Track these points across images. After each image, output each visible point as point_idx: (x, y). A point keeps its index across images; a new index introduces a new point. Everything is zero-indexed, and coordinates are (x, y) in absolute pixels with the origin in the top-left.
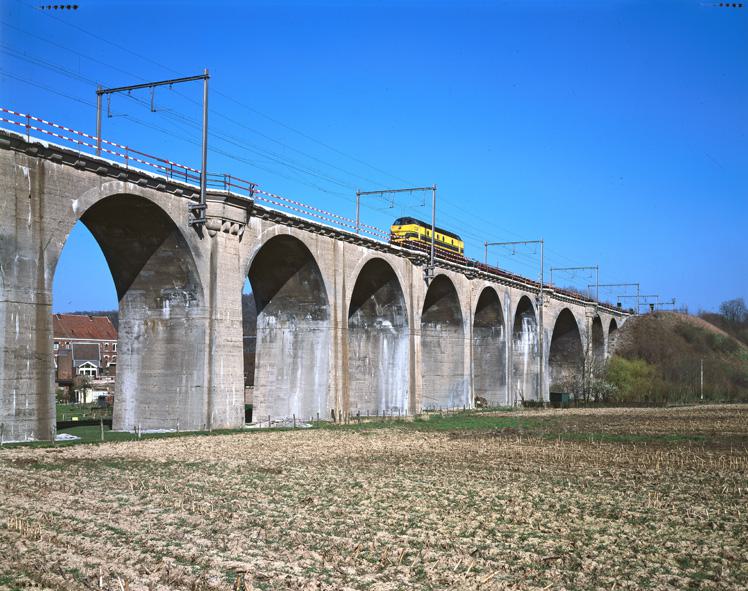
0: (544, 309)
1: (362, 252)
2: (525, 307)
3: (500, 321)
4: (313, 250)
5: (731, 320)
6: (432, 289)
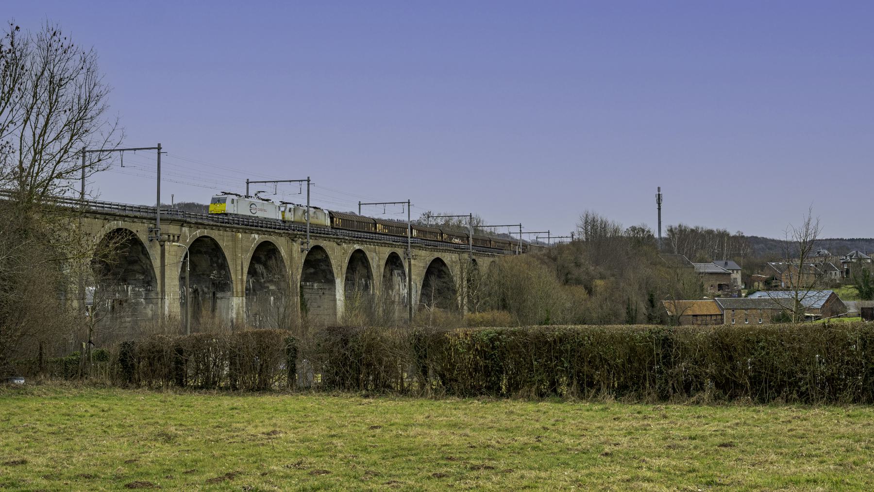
0: (412, 262)
1: (255, 239)
3: (369, 276)
4: (220, 243)
6: (308, 263)
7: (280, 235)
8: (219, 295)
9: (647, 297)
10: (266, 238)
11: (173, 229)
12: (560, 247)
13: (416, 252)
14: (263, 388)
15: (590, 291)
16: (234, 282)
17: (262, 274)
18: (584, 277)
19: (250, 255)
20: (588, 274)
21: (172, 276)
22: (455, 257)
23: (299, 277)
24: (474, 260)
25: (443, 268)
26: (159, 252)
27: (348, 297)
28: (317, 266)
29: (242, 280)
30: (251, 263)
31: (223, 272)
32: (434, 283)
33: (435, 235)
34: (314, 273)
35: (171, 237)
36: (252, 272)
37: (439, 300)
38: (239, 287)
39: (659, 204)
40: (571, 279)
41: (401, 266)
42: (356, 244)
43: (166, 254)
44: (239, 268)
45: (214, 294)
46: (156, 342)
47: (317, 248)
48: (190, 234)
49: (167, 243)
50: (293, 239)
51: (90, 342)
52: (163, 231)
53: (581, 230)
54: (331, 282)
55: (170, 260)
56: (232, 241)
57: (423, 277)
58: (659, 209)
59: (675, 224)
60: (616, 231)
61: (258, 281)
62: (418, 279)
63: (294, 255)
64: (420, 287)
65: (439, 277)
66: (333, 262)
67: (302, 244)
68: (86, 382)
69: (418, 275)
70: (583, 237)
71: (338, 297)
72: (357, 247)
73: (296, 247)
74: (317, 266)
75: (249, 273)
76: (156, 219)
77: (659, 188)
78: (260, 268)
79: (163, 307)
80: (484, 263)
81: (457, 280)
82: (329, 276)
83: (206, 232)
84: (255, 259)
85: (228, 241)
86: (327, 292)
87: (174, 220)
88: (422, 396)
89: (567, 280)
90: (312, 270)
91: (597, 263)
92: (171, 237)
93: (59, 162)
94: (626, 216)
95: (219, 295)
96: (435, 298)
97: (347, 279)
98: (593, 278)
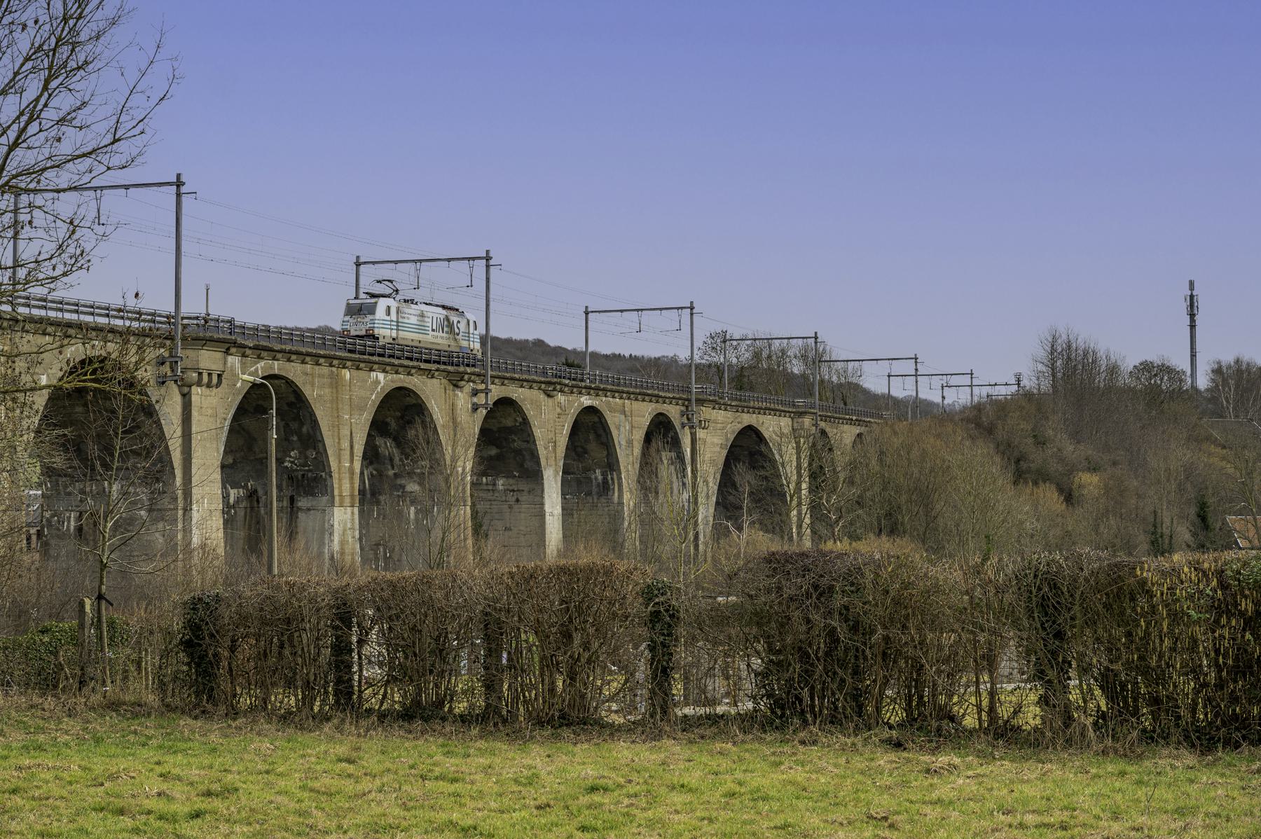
0: (701, 434)
1: (377, 382)
2: (660, 431)
3: (611, 465)
4: (307, 391)
5: (1246, 385)
6: (488, 436)
7: (430, 374)
8: (303, 503)
9: (1193, 511)
10: (401, 380)
11: (208, 359)
12: (1001, 407)
13: (707, 412)
14: (571, 719)
15: (1069, 497)
16: (335, 475)
17: (391, 460)
18: (1054, 467)
19: (366, 418)
20: (1061, 460)
21: (208, 457)
22: (785, 423)
23: (469, 466)
24: (823, 432)
25: (763, 448)
26: (179, 409)
27: (567, 512)
28: (505, 442)
29: (352, 472)
30: (370, 436)
31: (312, 454)
32: (746, 479)
33: (755, 377)
34: (499, 457)
35: (205, 378)
36: (371, 456)
37: (755, 517)
38: (346, 485)
39: (1192, 316)
40: (1029, 471)
41: (676, 444)
42: (527, 414)
43: (195, 413)
44: (345, 444)
45: (292, 500)
46: (282, 598)
47: (506, 403)
48: (245, 373)
49: (196, 390)
50: (456, 382)
51: (100, 597)
52: (189, 364)
53: (1041, 367)
54: (535, 476)
55: (200, 426)
56: (331, 385)
57: (721, 466)
58: (1193, 326)
59: (1228, 358)
60: (1113, 370)
61: (381, 474)
62: (712, 470)
63: (455, 413)
64: (713, 487)
65: (753, 467)
66: (538, 433)
67: (475, 393)
68: (751, 736)
69: (713, 462)
70: (1046, 385)
71: (547, 508)
72: (586, 401)
73: (462, 399)
74: (505, 442)
75: (365, 457)
76: (172, 338)
77: (1191, 284)
78: (386, 446)
79: (187, 531)
80: (845, 435)
81: (790, 471)
82: (529, 464)
83: (277, 367)
84: (378, 426)
85: (322, 387)
86: (523, 498)
87: (212, 340)
88: (1069, 742)
89: (1023, 472)
90: (493, 451)
91: (1076, 436)
92: (205, 378)
93: (16, 144)
94: (1134, 337)
95: (303, 503)
96: (750, 513)
97: (566, 471)
98: (1071, 470)
